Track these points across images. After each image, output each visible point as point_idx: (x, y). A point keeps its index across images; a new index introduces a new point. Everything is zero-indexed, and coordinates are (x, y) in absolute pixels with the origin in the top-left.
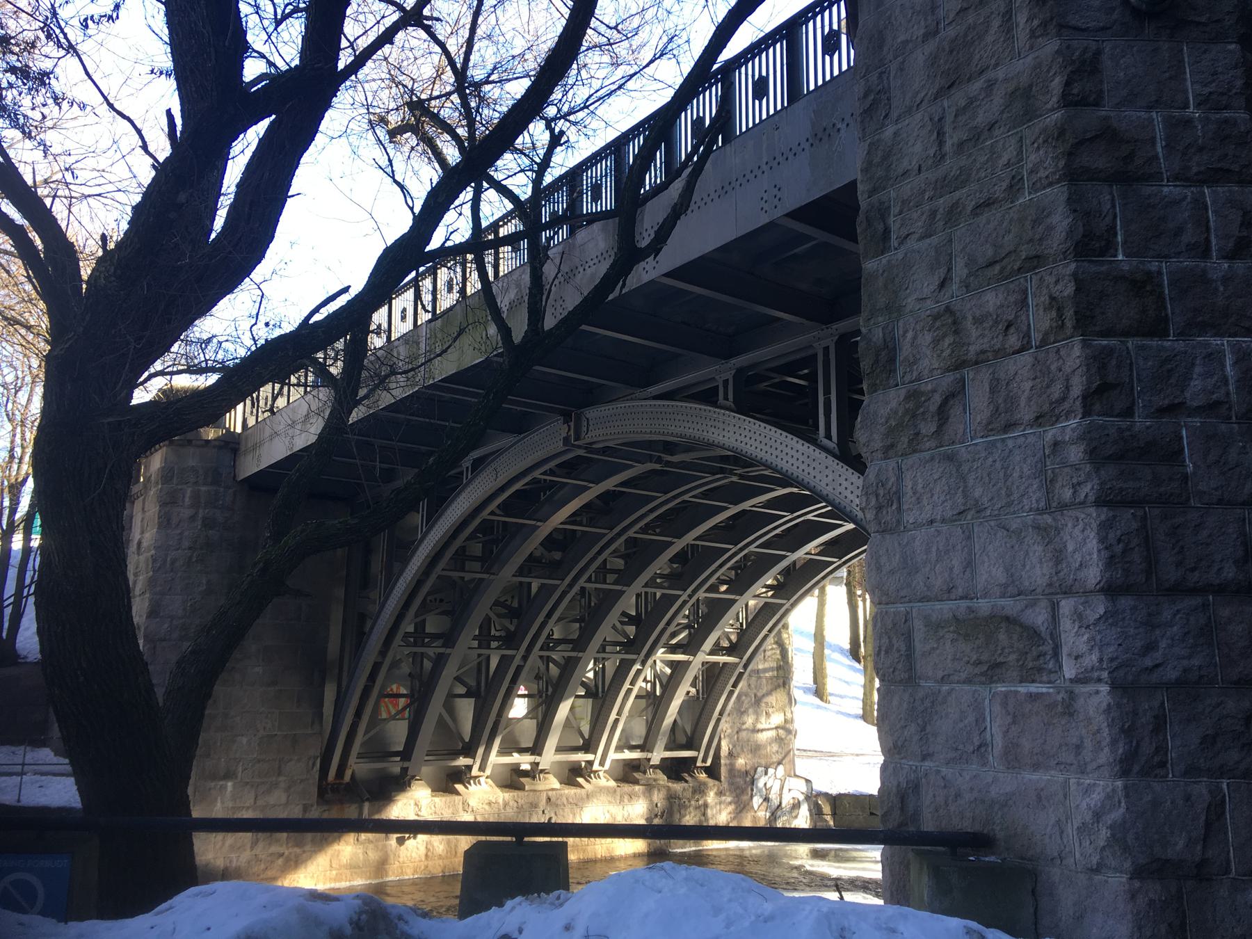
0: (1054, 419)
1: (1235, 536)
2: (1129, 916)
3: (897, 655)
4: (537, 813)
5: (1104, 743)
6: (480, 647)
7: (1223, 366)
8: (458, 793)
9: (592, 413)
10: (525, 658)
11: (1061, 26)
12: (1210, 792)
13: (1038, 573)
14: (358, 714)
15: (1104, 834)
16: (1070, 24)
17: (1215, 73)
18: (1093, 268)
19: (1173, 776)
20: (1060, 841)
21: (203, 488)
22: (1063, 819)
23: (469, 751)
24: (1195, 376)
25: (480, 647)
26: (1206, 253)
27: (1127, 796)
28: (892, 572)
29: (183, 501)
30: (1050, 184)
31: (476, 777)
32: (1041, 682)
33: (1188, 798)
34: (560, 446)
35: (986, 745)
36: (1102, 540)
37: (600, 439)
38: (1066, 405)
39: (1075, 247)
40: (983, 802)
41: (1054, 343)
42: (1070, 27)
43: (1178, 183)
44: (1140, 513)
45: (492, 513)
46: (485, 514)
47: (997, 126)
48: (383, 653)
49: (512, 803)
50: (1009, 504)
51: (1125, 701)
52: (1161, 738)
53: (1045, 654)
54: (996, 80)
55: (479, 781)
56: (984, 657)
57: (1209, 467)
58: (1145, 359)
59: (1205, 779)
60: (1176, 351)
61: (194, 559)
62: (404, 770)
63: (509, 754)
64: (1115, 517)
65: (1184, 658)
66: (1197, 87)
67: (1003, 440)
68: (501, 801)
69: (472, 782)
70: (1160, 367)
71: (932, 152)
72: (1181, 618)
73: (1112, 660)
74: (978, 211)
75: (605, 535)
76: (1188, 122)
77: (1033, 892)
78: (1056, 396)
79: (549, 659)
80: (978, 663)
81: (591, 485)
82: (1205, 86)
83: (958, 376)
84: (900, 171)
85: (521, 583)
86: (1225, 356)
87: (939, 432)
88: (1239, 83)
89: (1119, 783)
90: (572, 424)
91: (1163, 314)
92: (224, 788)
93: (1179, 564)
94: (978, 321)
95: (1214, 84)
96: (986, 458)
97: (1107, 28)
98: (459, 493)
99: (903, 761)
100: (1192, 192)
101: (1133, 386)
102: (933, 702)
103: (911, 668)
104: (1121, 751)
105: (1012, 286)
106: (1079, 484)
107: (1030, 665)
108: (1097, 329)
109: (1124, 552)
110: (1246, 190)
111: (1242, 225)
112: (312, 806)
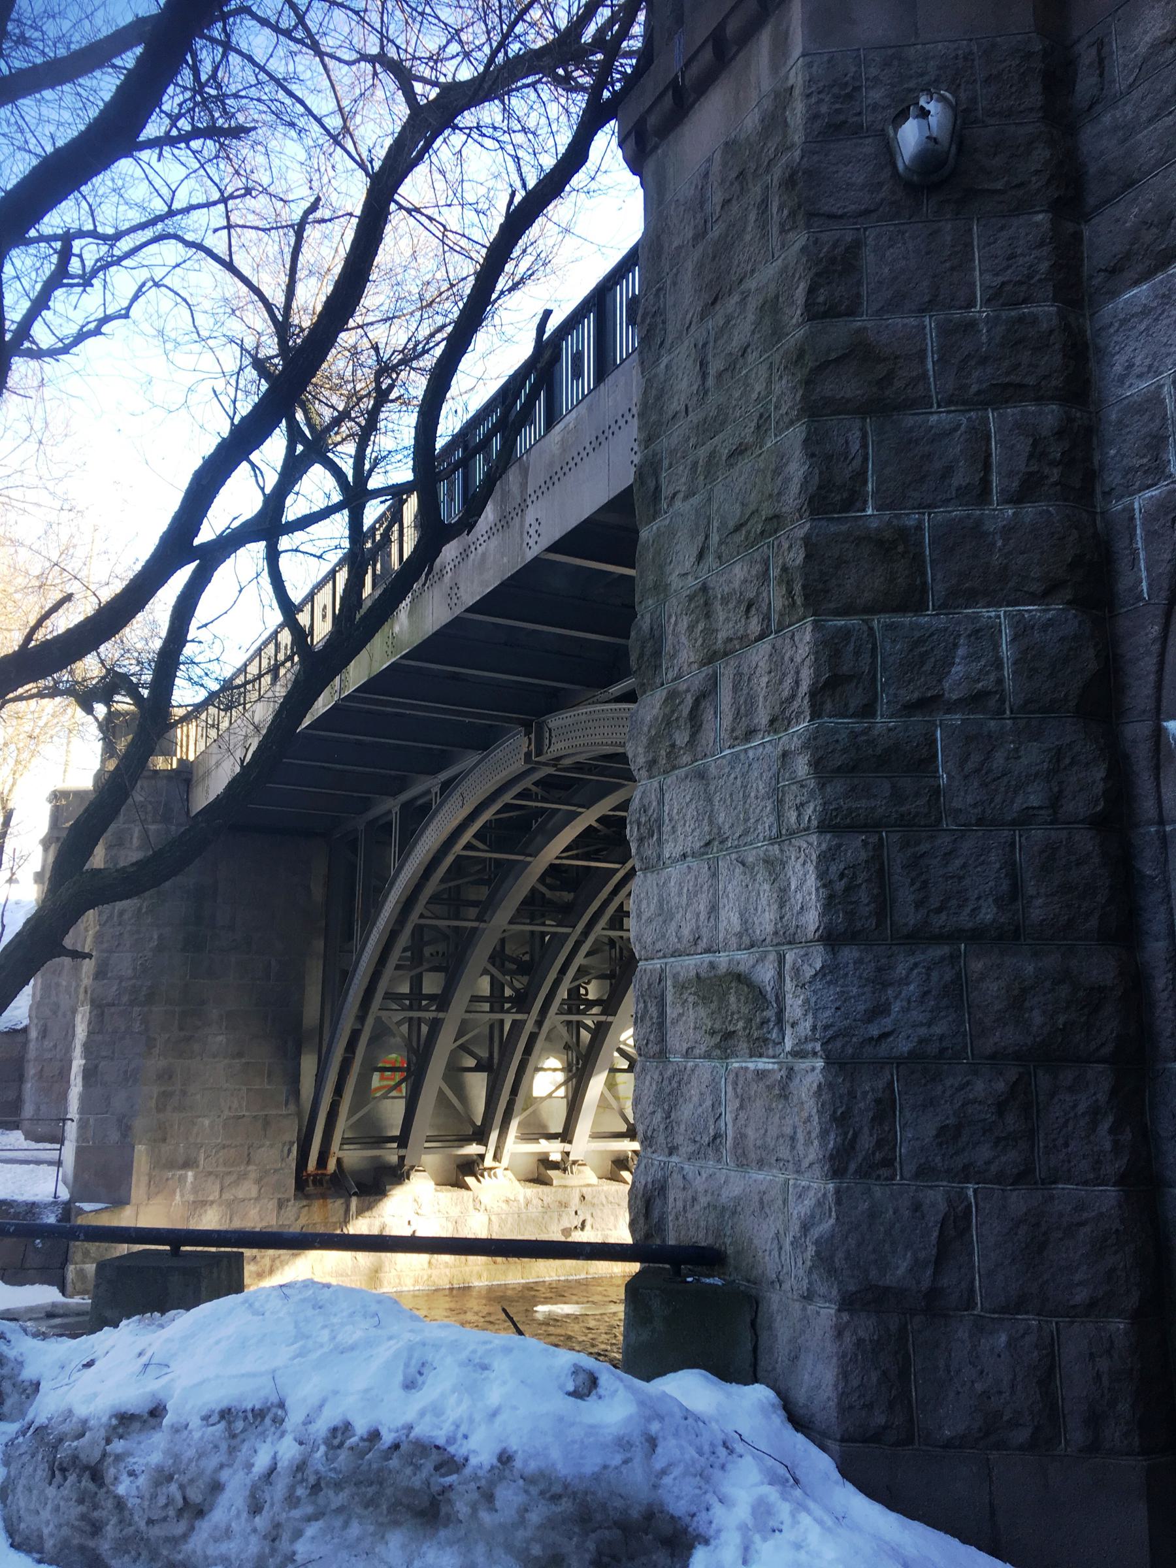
0: (786, 722)
1: (998, 865)
2: (835, 1360)
3: (649, 1024)
4: (568, 1214)
5: (814, 1135)
6: (492, 1011)
7: (996, 646)
8: (468, 1188)
9: (555, 722)
10: (539, 1023)
11: (811, 215)
12: (949, 1202)
13: (766, 921)
14: (339, 1091)
15: (811, 1250)
16: (821, 212)
17: (1012, 256)
18: (833, 528)
19: (902, 1178)
20: (777, 1260)
21: (152, 827)
22: (782, 1232)
23: (480, 1136)
24: (957, 660)
25: (492, 1011)
26: (982, 494)
27: (838, 1202)
28: (650, 920)
29: (131, 843)
30: (792, 423)
31: (491, 1169)
32: (768, 1057)
33: (917, 1207)
34: (519, 765)
35: (720, 1136)
36: (820, 877)
37: (570, 751)
38: (795, 705)
39: (810, 502)
40: (715, 1207)
41: (790, 626)
42: (823, 215)
43: (953, 408)
44: (874, 839)
45: (469, 846)
46: (458, 848)
47: (749, 350)
48: (361, 1018)
49: (536, 1201)
50: (746, 832)
51: (840, 1080)
52: (887, 1129)
53: (769, 1020)
54: (750, 290)
55: (495, 1175)
56: (717, 1026)
57: (966, 777)
58: (894, 641)
59: (945, 1183)
60: (933, 628)
61: (144, 910)
62: (402, 1158)
63: (536, 1140)
64: (839, 846)
65: (922, 1024)
66: (987, 277)
67: (746, 750)
68: (522, 1200)
69: (486, 1174)
70: (911, 650)
71: (695, 387)
72: (919, 973)
73: (826, 1028)
74: (732, 461)
75: (617, 870)
76: (970, 326)
77: (753, 1324)
78: (786, 694)
79: (579, 1024)
80: (713, 1033)
81: (580, 810)
82: (997, 275)
83: (710, 671)
84: (670, 414)
85: (532, 933)
86: (1000, 631)
87: (692, 742)
88: (1044, 266)
89: (831, 1186)
90: (533, 736)
91: (918, 582)
92: (183, 1179)
93: (919, 904)
94: (725, 601)
95: (1009, 271)
96: (729, 775)
97: (872, 211)
98: (427, 825)
99: (655, 1156)
100: (969, 419)
101: (875, 676)
102: (679, 1082)
103: (662, 1040)
104: (831, 1145)
105: (756, 555)
106: (802, 805)
107: (755, 1035)
108: (832, 606)
109: (847, 889)
110: (1046, 409)
111: (1031, 456)
112: (288, 1200)
